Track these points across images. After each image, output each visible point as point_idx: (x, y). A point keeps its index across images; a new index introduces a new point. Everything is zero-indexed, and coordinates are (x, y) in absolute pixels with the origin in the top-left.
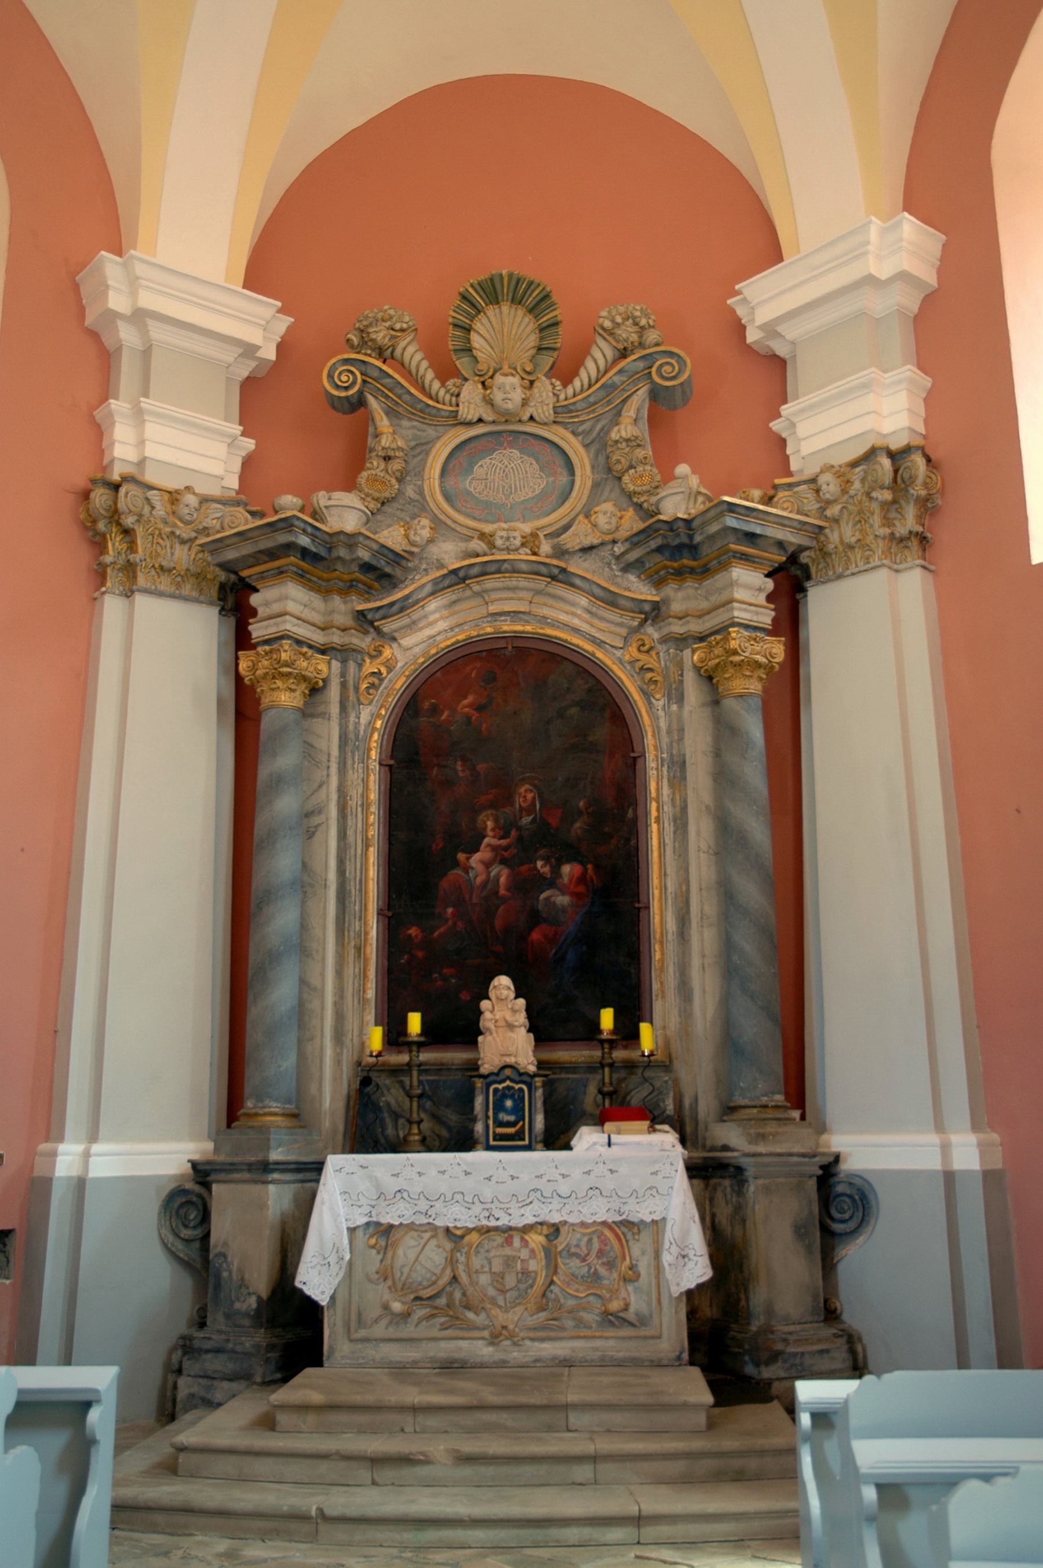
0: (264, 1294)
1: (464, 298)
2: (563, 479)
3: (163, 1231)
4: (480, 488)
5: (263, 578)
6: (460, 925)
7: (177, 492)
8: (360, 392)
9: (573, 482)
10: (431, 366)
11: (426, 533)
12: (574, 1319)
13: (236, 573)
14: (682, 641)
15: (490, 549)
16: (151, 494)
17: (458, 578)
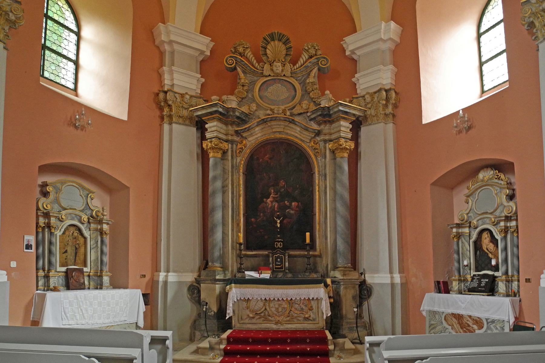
0: (216, 311)
1: (264, 39)
2: (293, 93)
3: (188, 295)
5: (209, 120)
6: (265, 218)
7: (183, 94)
9: (296, 94)
11: (255, 108)
12: (297, 319)
13: (201, 118)
14: (325, 141)
15: (273, 113)
16: (176, 95)
17: (264, 121)
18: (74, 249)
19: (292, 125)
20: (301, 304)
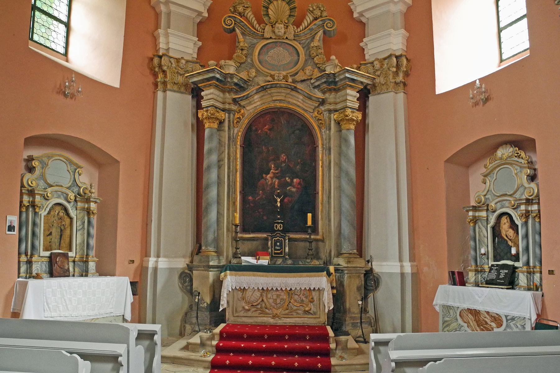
2: (296, 58)
4: (270, 60)
8: (234, 27)
10: (256, 19)
11: (254, 74)
14: (330, 111)
15: (273, 80)
16: (171, 60)
17: (263, 89)
19: (294, 93)
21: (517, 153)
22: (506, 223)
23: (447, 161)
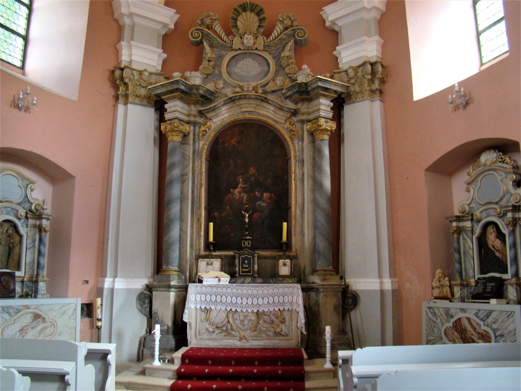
2: (266, 68)
8: (201, 40)
9: (269, 70)
11: (222, 85)
14: (303, 122)
16: (134, 72)
17: (232, 100)
18: (7, 248)
19: (265, 105)
20: (272, 315)
21: (502, 159)
22: (493, 233)
23: (427, 170)
